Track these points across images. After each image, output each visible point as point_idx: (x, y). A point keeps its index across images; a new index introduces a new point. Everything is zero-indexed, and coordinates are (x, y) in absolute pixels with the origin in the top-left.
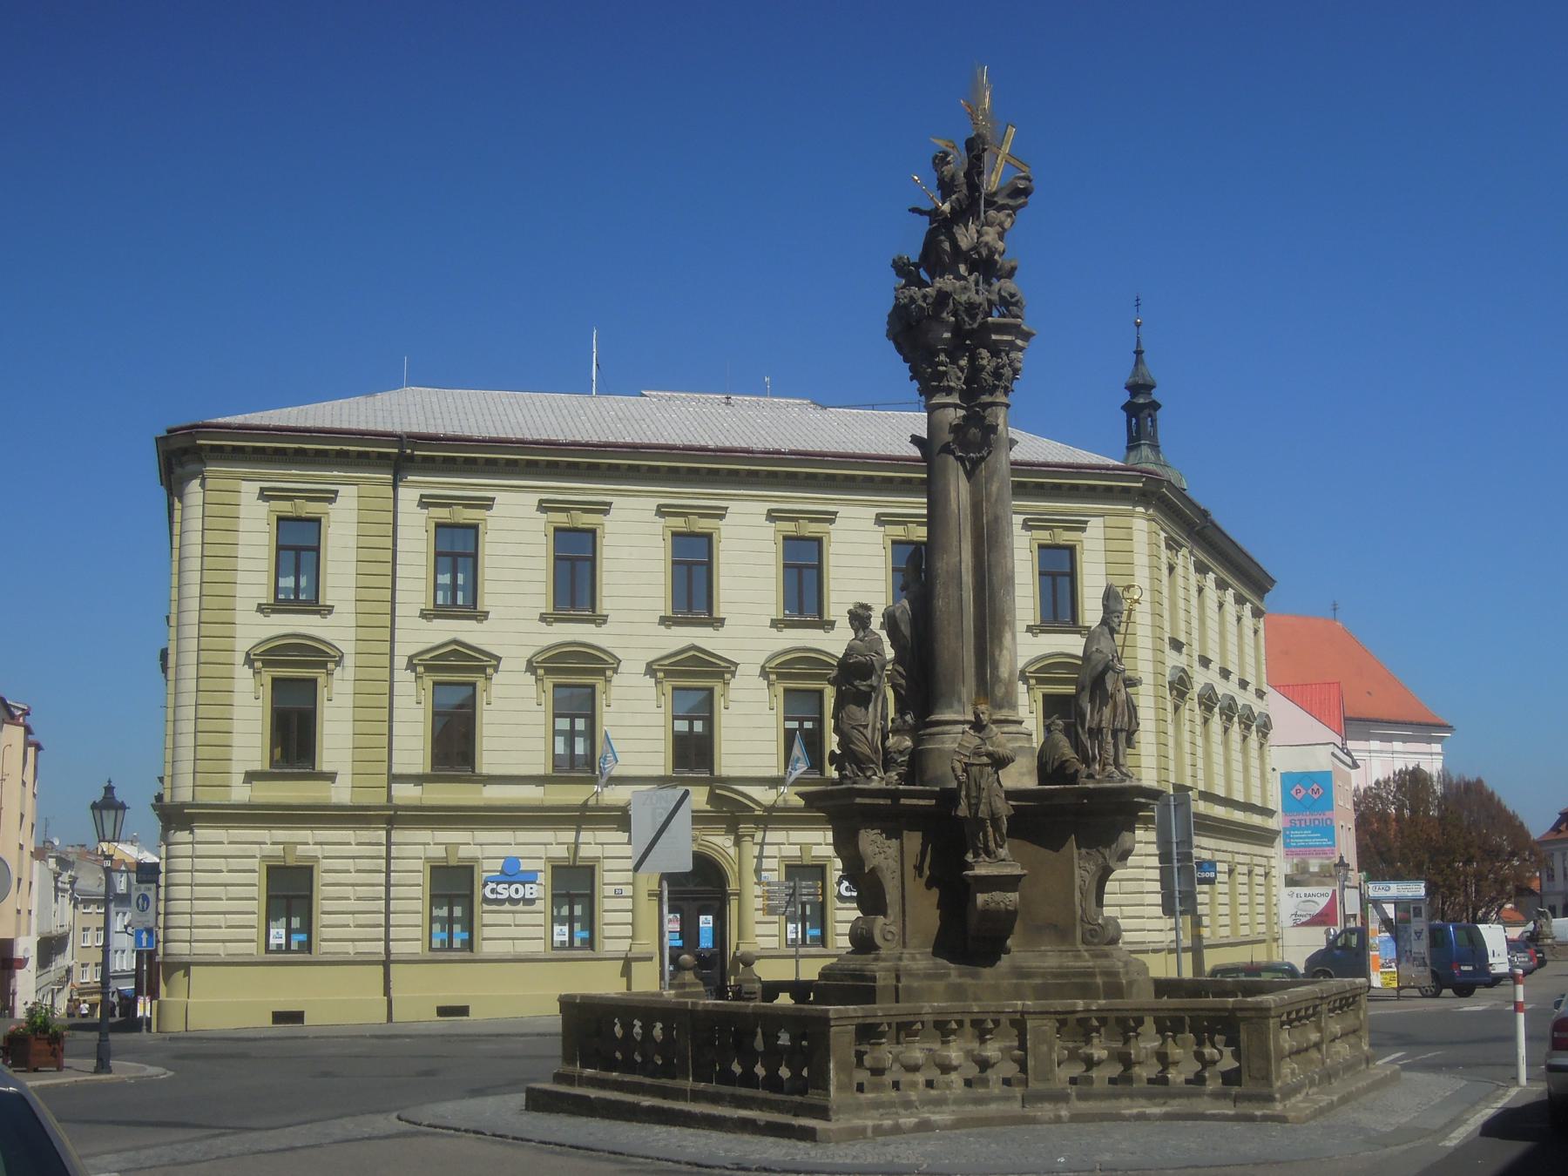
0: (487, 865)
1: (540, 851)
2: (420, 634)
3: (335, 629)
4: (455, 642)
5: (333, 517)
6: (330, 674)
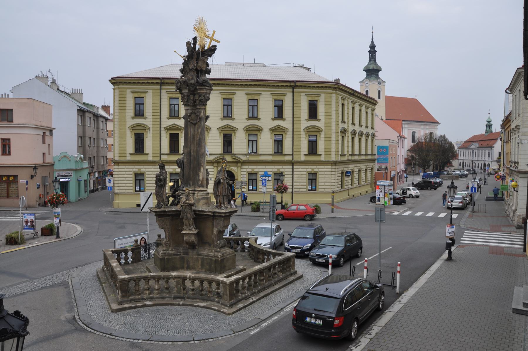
1: (271, 170)
2: (131, 122)
3: (286, 123)
4: (228, 125)
5: (320, 100)
6: (147, 132)
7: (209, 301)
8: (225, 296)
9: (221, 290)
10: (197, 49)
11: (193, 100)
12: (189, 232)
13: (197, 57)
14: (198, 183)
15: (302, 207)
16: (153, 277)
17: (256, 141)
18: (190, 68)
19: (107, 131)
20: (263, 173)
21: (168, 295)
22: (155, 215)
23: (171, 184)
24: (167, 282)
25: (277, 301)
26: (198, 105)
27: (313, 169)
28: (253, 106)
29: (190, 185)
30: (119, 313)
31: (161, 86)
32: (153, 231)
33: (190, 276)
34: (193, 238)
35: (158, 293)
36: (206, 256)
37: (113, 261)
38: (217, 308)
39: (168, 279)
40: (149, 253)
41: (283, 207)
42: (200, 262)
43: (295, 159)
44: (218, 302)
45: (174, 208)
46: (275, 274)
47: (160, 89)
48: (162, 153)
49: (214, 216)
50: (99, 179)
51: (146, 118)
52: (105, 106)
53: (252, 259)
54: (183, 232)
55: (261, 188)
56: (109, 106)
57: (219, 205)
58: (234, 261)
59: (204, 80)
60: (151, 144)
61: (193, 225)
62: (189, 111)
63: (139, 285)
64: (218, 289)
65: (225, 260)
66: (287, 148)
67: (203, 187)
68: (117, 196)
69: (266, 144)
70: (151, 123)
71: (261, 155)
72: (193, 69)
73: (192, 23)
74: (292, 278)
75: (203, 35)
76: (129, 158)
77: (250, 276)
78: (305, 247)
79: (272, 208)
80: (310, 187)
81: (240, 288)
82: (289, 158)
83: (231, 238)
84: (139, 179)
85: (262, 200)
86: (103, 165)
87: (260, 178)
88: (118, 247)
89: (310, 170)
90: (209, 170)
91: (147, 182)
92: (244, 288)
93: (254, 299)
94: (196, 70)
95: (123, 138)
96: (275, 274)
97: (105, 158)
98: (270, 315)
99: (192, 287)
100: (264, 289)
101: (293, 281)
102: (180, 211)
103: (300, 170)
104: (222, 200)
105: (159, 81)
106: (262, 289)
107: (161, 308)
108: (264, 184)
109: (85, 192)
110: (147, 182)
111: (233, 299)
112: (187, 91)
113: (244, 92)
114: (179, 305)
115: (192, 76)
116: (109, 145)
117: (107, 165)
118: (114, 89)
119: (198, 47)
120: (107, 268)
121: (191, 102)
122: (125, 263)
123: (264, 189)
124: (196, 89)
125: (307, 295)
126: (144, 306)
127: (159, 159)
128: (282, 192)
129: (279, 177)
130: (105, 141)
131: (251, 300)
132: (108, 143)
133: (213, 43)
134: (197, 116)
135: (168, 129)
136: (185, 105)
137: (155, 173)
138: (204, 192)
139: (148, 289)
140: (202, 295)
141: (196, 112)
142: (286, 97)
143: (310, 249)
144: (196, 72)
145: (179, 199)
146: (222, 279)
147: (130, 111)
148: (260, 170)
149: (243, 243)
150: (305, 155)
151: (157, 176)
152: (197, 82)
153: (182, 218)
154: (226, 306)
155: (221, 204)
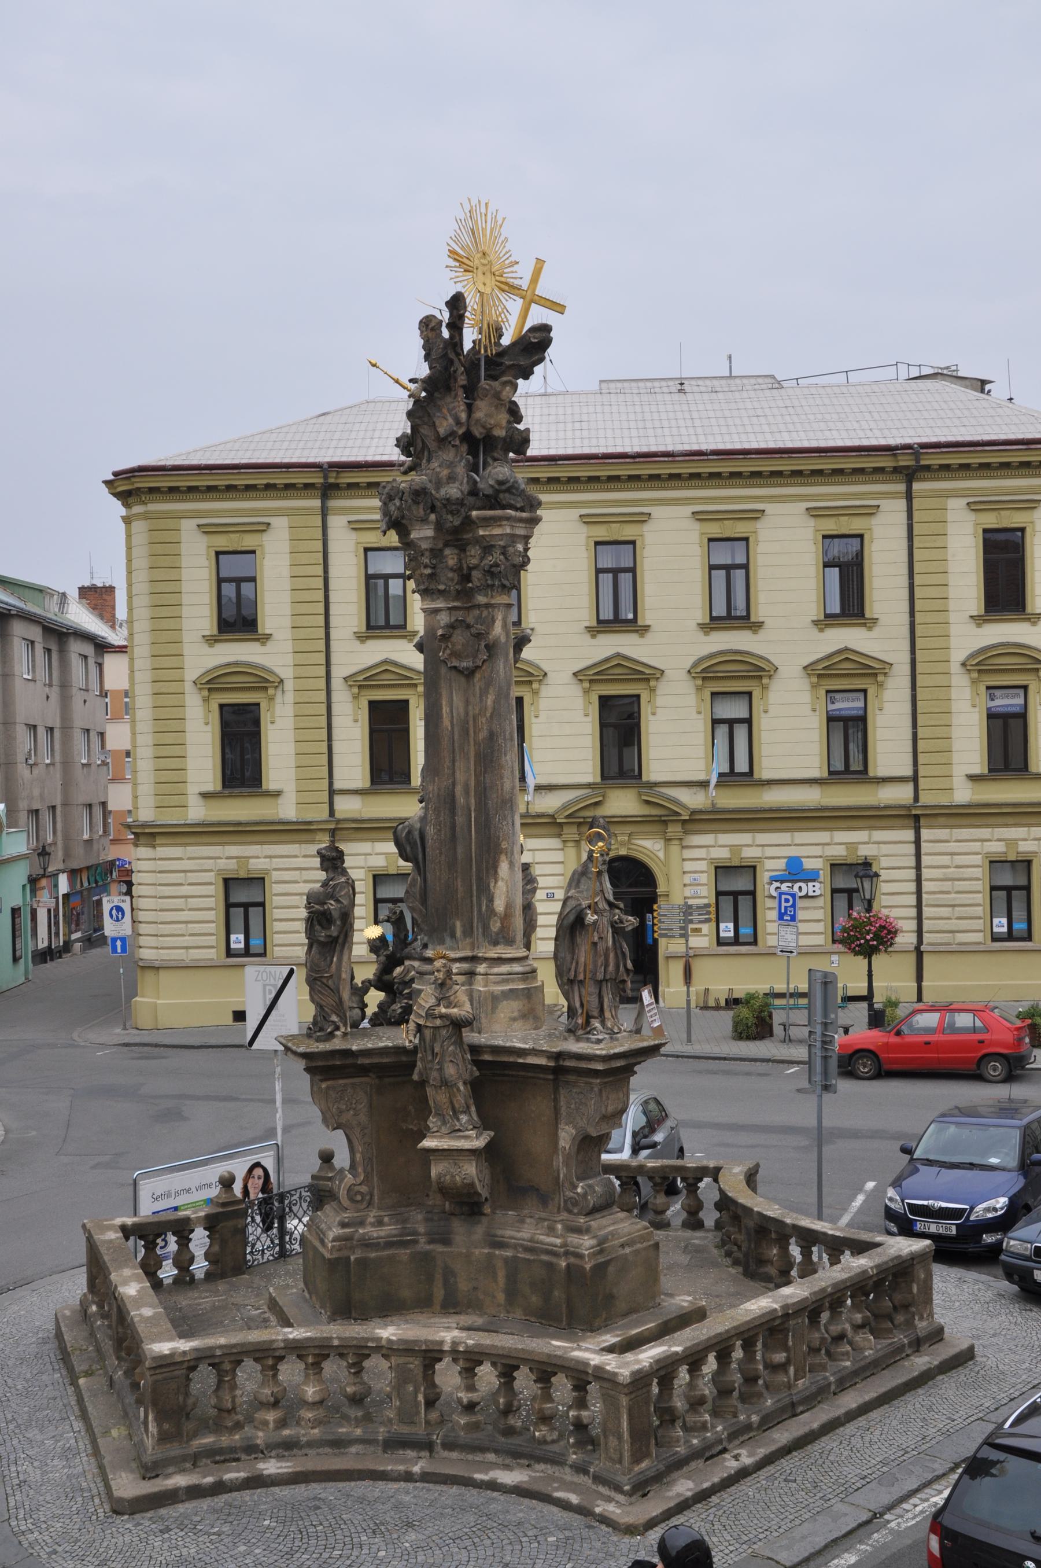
0: (769, 864)
1: (817, 851)
2: (202, 657)
3: (882, 639)
4: (618, 655)
6: (272, 699)
7: (539, 1460)
8: (613, 1442)
9: (595, 1409)
10: (467, 346)
11: (458, 569)
12: (454, 1140)
13: (471, 376)
14: (486, 928)
15: (964, 1020)
16: (297, 1348)
17: (748, 721)
18: (442, 431)
19: (104, 694)
20: (781, 864)
21: (358, 1432)
22: (308, 1070)
23: (374, 932)
24: (357, 1369)
25: (851, 1473)
26: (478, 589)
27: (1011, 843)
28: (728, 568)
29: (453, 935)
30: (145, 1519)
31: (324, 497)
32: (297, 1137)
33: (455, 1343)
34: (470, 1170)
35: (317, 1423)
36: (527, 1249)
37: (127, 1272)
38: (574, 1499)
39: (358, 1354)
40: (283, 1231)
41: (876, 1019)
42: (501, 1275)
43: (925, 799)
44: (581, 1469)
45: (388, 1038)
46: (840, 1338)
47: (324, 513)
48: (337, 785)
49: (561, 1070)
50: (75, 901)
51: (266, 638)
52: (93, 588)
53: (736, 1263)
54: (428, 1143)
55: (772, 931)
56: (111, 590)
57: (580, 1021)
58: (652, 1274)
59: (501, 483)
60: (290, 749)
61: (467, 1111)
62: (444, 619)
63: (234, 1387)
64: (581, 1403)
65: (611, 1269)
66: (889, 749)
67: (510, 942)
68: (150, 976)
69: (791, 737)
70: (289, 659)
71: (770, 783)
72: (453, 434)
73: (442, 229)
74: (922, 1362)
75: (491, 282)
76: (197, 812)
77: (722, 1348)
78: (981, 1211)
79: (818, 1029)
80: (1001, 925)
81: (679, 1403)
82: (902, 794)
83: (641, 1168)
84: (243, 901)
85: (780, 987)
86: (89, 842)
87: (767, 889)
88: (147, 1209)
89: (997, 848)
90: (537, 870)
91: (278, 914)
92: (696, 1403)
93: (747, 1460)
94: (468, 438)
95: (169, 727)
96: (840, 1338)
97: (98, 812)
98: (820, 1541)
99: (465, 1396)
100: (790, 1411)
101: (924, 1378)
102: (415, 1050)
103: (953, 847)
104: (594, 1000)
105: (317, 479)
106: (782, 1410)
107: (328, 1491)
108: (787, 916)
109: (15, 959)
110: (278, 914)
111: (647, 1455)
112: (429, 532)
113: (689, 510)
114: (408, 1477)
115: (451, 465)
116: (116, 752)
117: (106, 841)
118: (127, 520)
119: (469, 337)
120: (101, 1306)
121: (448, 580)
122: (177, 1281)
123: (788, 937)
124: (468, 523)
125: (994, 1455)
126: (257, 1482)
127: (325, 815)
128: (868, 952)
129: (854, 879)
130: (94, 738)
131: (731, 1465)
132: (109, 746)
133: (538, 316)
134: (479, 636)
135: (363, 681)
136: (425, 593)
137: (306, 888)
138: (517, 968)
139: (275, 1404)
140: (510, 1432)
141: (470, 620)
142: (875, 521)
143: (1006, 1222)
144: (464, 448)
145: (409, 996)
146: (595, 1359)
147: (199, 613)
148: (770, 852)
149: (692, 1188)
150: (973, 778)
151: (312, 899)
152: (474, 492)
153: (423, 1083)
154: (618, 1489)
155: (589, 1018)
